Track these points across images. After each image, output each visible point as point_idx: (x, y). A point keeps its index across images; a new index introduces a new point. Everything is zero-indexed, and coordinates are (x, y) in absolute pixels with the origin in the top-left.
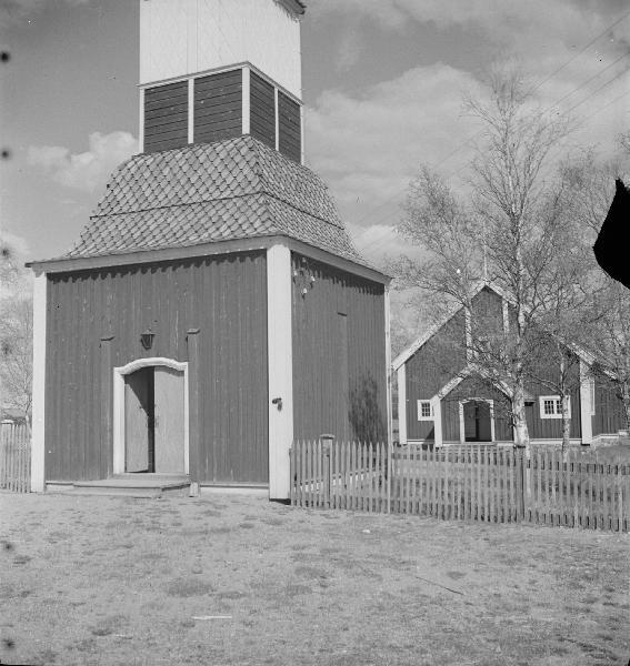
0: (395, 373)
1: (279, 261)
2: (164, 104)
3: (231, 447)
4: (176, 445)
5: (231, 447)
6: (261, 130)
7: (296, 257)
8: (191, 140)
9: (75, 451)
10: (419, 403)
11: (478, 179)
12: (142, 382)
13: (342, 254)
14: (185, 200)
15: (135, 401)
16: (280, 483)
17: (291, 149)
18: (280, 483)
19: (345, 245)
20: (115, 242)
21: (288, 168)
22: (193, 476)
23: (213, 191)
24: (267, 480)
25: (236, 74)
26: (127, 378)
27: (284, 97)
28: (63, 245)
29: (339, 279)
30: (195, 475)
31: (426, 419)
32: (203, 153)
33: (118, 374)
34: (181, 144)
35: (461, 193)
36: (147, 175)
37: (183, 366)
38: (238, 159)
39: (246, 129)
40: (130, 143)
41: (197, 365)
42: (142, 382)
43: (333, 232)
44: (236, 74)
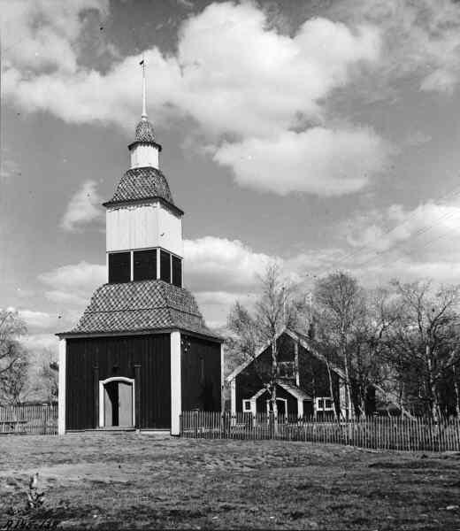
0: (228, 387)
1: (176, 339)
2: (118, 264)
3: (153, 413)
4: (128, 414)
5: (153, 413)
6: (165, 277)
7: (182, 336)
8: (132, 279)
9: (82, 416)
10: (244, 401)
11: (259, 307)
12: (112, 390)
13: (202, 331)
14: (131, 308)
15: (109, 403)
16: (176, 426)
17: (178, 282)
18: (176, 426)
19: (203, 326)
20: (97, 325)
21: (177, 293)
22: (137, 427)
23: (140, 308)
24: (170, 427)
25: (154, 251)
26: (104, 385)
27: (165, 255)
28: (73, 322)
29: (203, 347)
30: (137, 427)
31: (248, 411)
32: (139, 287)
33: (101, 383)
34: (127, 280)
35: (252, 312)
36: (112, 294)
37: (132, 381)
38: (156, 291)
39: (159, 276)
40: (103, 272)
41: (139, 381)
42: (112, 390)
43: (196, 319)
44: (154, 251)
